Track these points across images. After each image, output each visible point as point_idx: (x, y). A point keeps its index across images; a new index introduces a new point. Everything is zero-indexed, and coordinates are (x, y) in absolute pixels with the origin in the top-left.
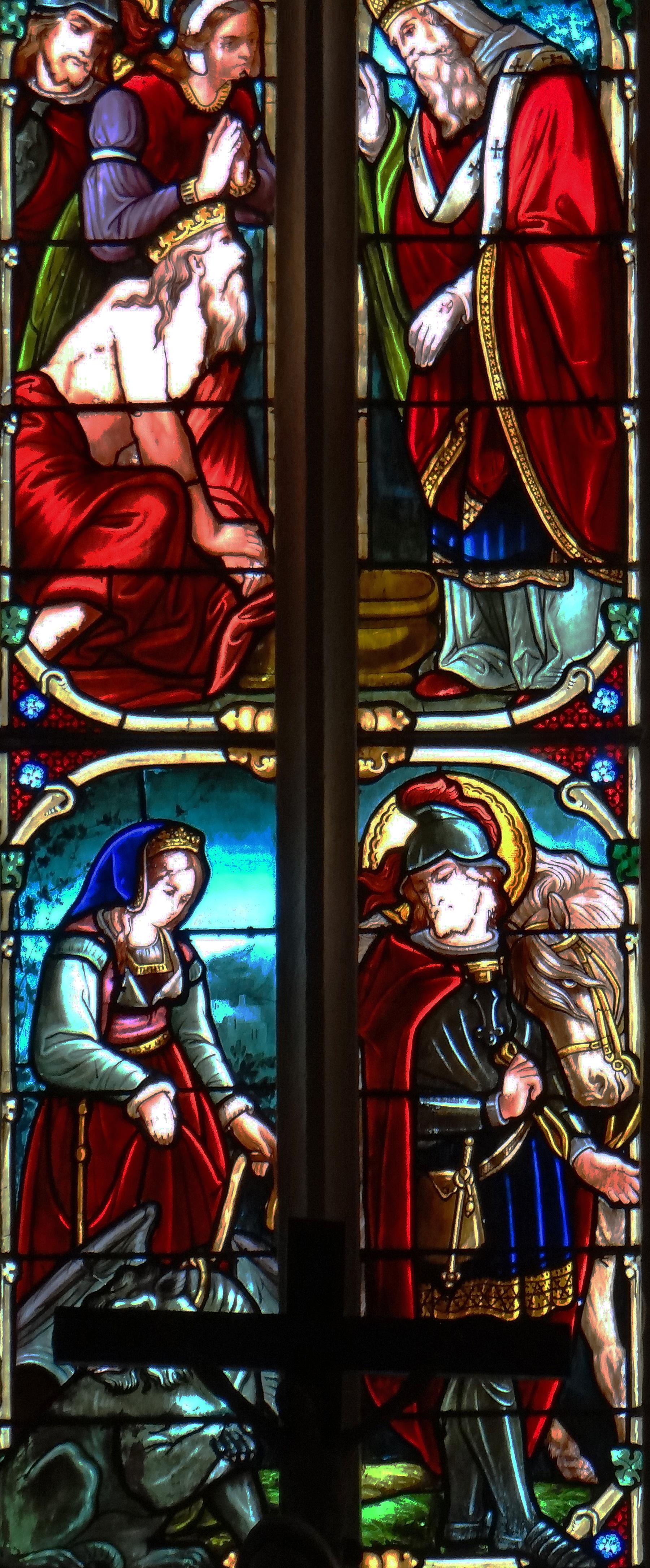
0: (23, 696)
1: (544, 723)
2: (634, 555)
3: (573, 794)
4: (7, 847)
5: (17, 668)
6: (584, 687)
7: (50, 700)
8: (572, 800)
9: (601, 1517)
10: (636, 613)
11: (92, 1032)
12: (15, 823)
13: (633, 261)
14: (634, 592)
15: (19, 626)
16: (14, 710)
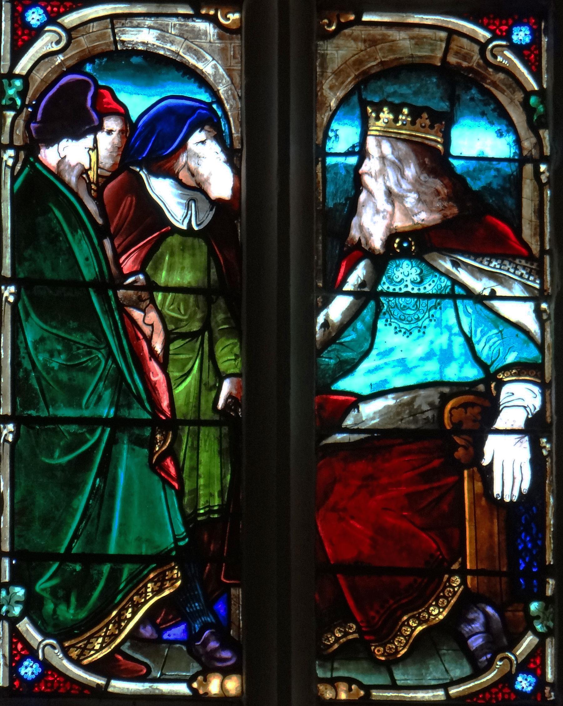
1: (472, 699)
3: (495, 51)
4: (11, 75)
5: (16, 636)
6: (509, 669)
7: (46, 665)
9: (520, 660)
11: (88, 140)
12: (17, 53)
15: (18, 602)
16: (13, 666)
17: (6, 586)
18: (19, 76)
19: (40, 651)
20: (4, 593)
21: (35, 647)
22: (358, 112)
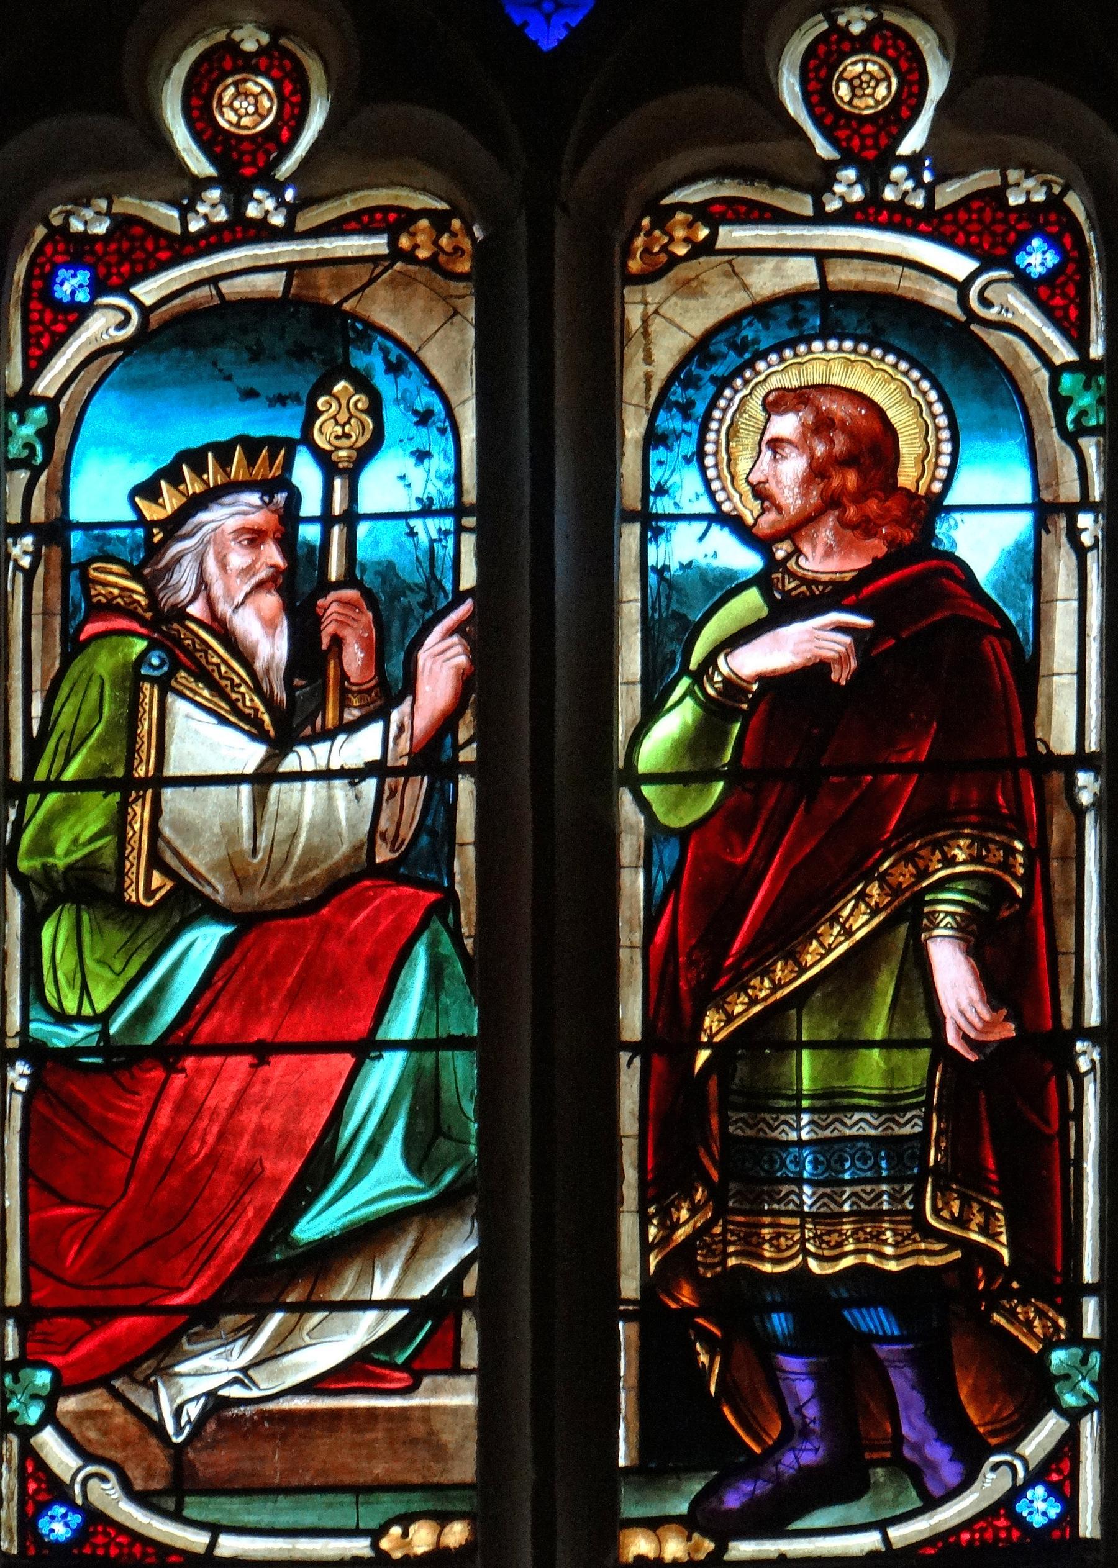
0: (42, 1508)
2: (1089, 1274)
5: (32, 1464)
8: (986, 303)
10: (1095, 1358)
13: (1093, 1068)
14: (1091, 1329)
15: (35, 1397)
16: (27, 1527)
17: (15, 1367)
18: (41, 400)
19: (77, 1489)
20: (8, 1380)
21: (67, 1479)
22: (685, 766)
